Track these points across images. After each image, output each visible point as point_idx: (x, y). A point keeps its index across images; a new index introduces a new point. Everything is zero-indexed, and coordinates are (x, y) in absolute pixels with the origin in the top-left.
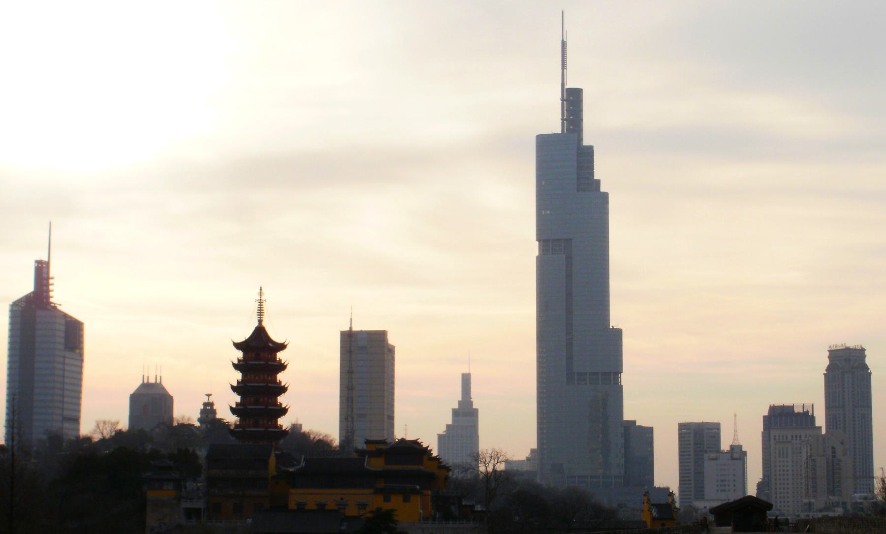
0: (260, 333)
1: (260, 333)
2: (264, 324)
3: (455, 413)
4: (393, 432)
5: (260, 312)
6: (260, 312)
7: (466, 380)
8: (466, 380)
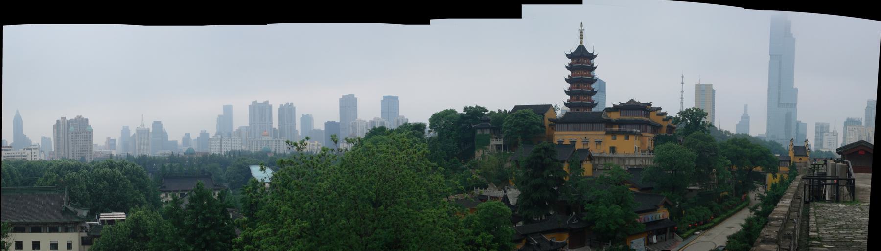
0: (581, 48)
1: (581, 48)
2: (584, 43)
3: (742, 118)
4: (22, 130)
5: (581, 37)
6: (581, 37)
7: (746, 106)
8: (746, 106)
